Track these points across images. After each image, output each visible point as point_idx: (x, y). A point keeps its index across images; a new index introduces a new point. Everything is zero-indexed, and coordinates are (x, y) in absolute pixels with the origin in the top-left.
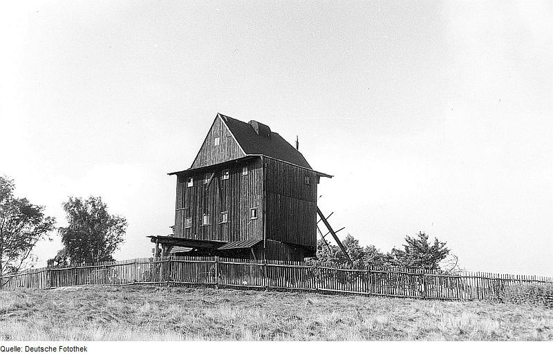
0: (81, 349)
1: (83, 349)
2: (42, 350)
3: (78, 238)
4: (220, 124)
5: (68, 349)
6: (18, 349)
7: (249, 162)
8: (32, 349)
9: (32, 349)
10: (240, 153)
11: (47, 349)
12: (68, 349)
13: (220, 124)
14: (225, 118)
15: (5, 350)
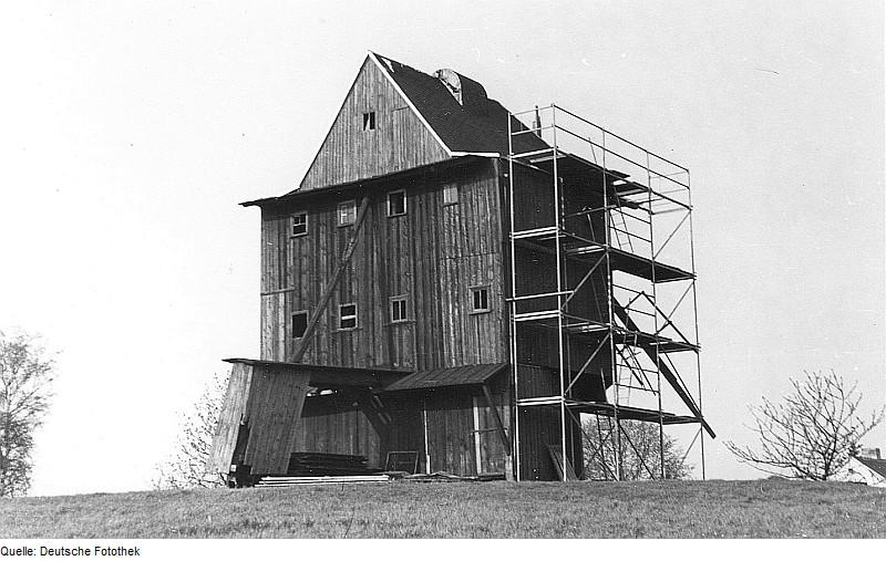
0: (131, 551)
1: (134, 552)
2: (68, 552)
3: (281, 416)
4: (376, 75)
5: (108, 552)
6: (29, 552)
7: (461, 172)
8: (51, 552)
9: (51, 552)
10: (437, 149)
11: (75, 552)
12: (108, 552)
13: (376, 75)
14: (389, 63)
15: (8, 553)
